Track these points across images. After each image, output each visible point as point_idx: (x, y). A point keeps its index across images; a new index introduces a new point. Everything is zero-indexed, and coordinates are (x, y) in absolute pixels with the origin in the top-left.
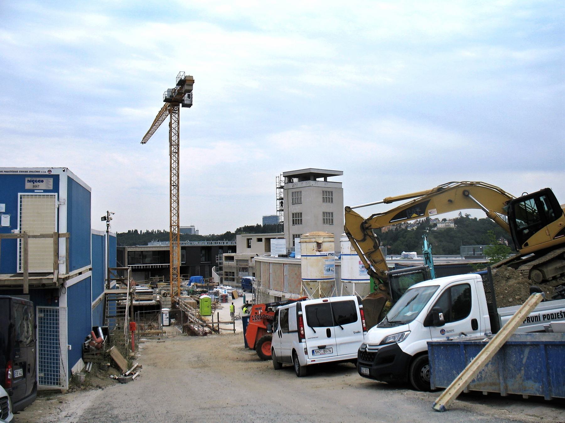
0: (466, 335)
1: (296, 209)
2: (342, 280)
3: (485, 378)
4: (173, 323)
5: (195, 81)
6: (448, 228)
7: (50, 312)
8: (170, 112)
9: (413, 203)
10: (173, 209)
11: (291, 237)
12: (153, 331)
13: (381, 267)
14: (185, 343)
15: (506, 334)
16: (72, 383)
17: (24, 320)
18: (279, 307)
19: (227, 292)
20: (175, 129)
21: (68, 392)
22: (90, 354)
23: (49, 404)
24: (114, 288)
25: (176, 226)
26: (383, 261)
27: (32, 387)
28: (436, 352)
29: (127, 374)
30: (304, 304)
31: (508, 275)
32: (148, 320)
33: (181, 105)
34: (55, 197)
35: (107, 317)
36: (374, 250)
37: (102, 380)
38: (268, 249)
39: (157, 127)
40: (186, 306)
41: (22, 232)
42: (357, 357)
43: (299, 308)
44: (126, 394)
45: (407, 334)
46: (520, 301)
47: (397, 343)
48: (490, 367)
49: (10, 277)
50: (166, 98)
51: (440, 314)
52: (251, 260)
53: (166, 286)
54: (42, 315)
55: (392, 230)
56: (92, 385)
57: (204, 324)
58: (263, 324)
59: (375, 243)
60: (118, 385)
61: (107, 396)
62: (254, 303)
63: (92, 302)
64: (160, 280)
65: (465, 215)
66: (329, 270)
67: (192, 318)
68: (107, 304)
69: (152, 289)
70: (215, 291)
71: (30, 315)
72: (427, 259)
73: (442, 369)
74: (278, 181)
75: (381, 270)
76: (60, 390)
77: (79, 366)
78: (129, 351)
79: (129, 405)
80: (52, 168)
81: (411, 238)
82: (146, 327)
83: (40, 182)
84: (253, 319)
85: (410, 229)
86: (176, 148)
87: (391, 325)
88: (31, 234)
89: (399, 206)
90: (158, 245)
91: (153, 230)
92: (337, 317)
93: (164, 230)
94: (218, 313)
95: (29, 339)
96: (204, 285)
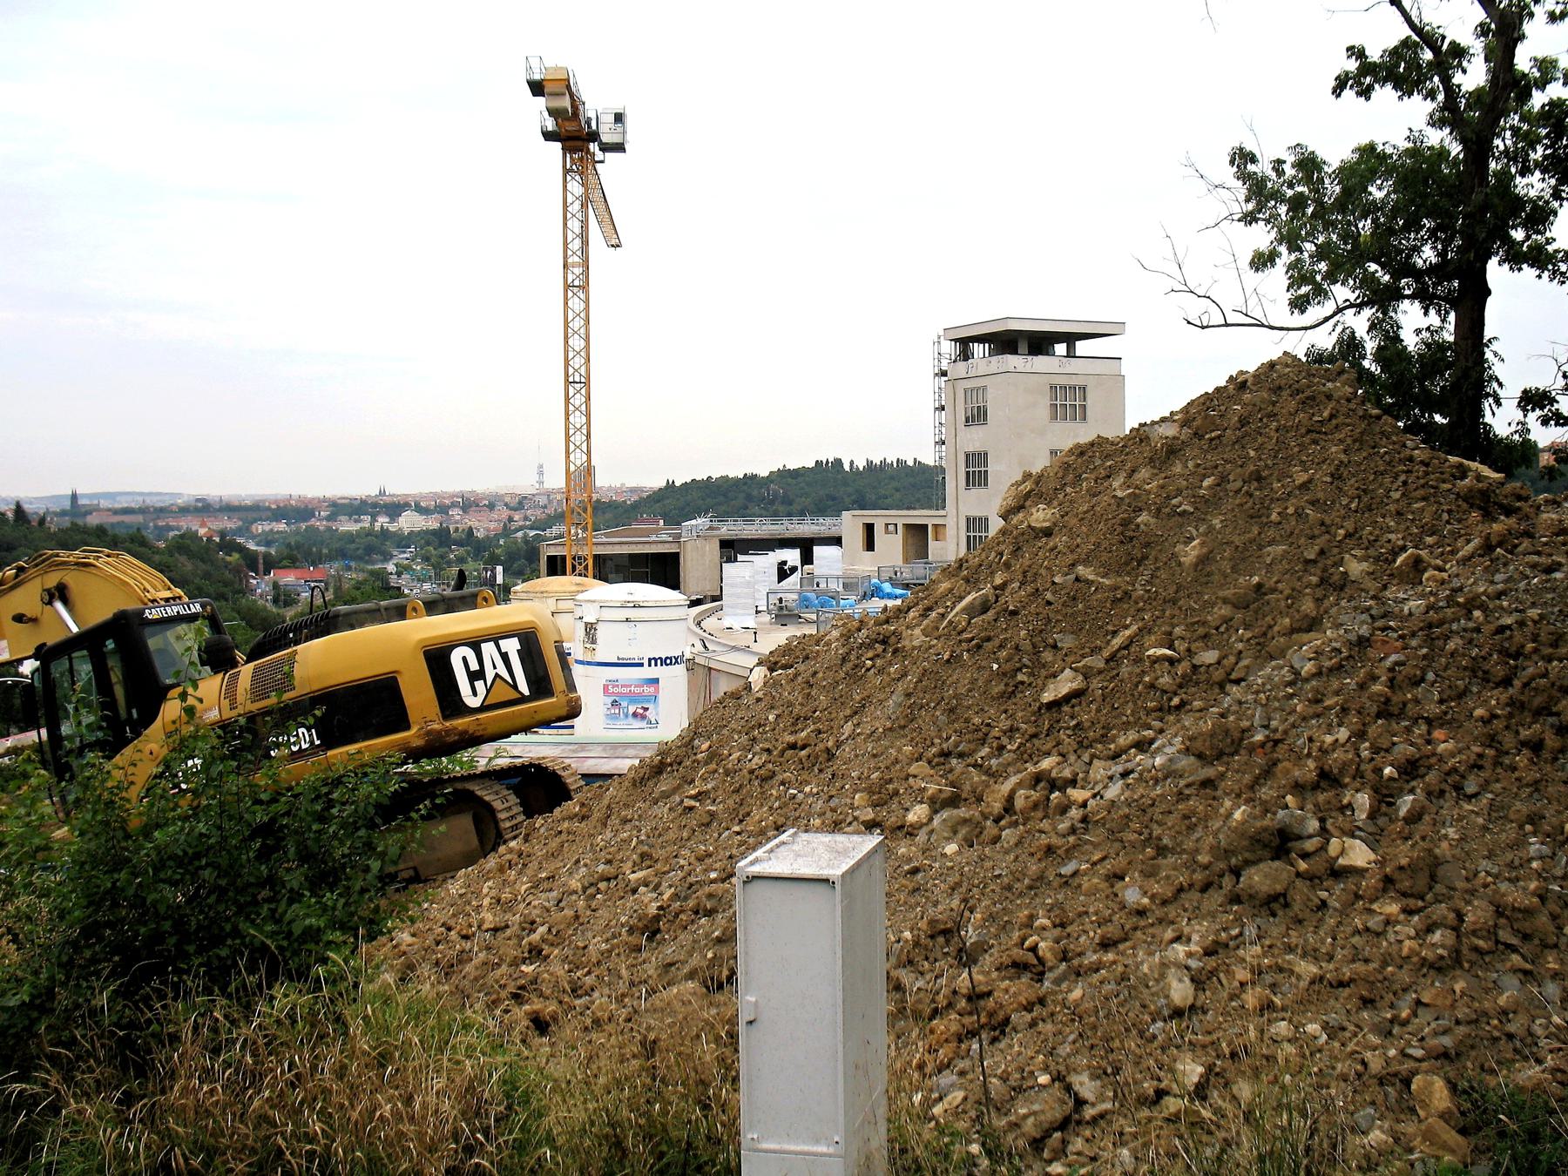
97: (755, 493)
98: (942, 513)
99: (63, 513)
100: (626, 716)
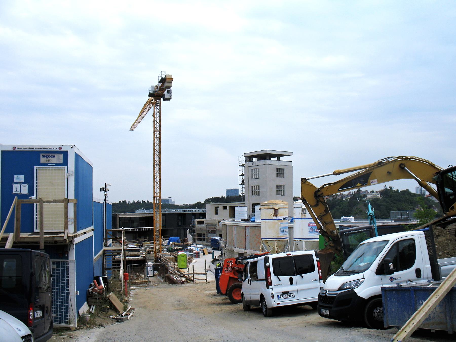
0: (412, 282)
1: (255, 183)
2: (294, 239)
3: (434, 318)
4: (156, 274)
5: (173, 79)
6: (375, 198)
7: (62, 264)
8: (154, 105)
9: (358, 174)
10: (156, 183)
11: (251, 205)
12: (140, 280)
13: (330, 227)
14: (167, 290)
15: (452, 281)
16: (80, 321)
17: (42, 270)
18: (248, 260)
19: (199, 250)
20: (157, 118)
21: (76, 329)
22: (94, 299)
23: (62, 339)
24: (110, 246)
25: (158, 196)
26: (332, 222)
27: (49, 325)
28: (388, 296)
29: (124, 314)
30: (271, 257)
31: (437, 233)
32: (136, 272)
33: (162, 99)
34: (64, 170)
35: (105, 269)
36: (325, 213)
37: (103, 320)
38: (232, 215)
39: (143, 117)
40: (166, 260)
41: (38, 198)
42: (318, 300)
43: (267, 260)
44: (124, 331)
45: (361, 281)
46: (448, 254)
47: (353, 289)
48: (438, 309)
49: (29, 235)
50: (150, 93)
51: (390, 264)
52: (218, 224)
53: (150, 245)
54: (55, 266)
55: (330, 200)
56: (95, 324)
57: (182, 275)
58: (234, 275)
59: (326, 208)
60: (117, 323)
61: (108, 333)
62: (221, 258)
63: (94, 256)
64: (145, 240)
65: (389, 188)
66: (284, 231)
67: (171, 270)
68: (105, 259)
69: (139, 247)
70: (189, 249)
71: (47, 266)
72: (372, 220)
73: (394, 311)
74: (240, 161)
75: (331, 230)
76: (70, 327)
77: (85, 308)
78: (123, 296)
79: (128, 340)
80: (62, 145)
81: (345, 206)
82: (136, 278)
83: (52, 157)
84: (225, 271)
85: (344, 199)
86: (158, 134)
87: (347, 274)
88: (45, 200)
89: (346, 177)
90: (144, 213)
91: (139, 201)
92: (298, 268)
93: (147, 201)
94: (193, 266)
95: (47, 286)
96: (180, 244)
98: (243, 202)
100: (314, 231)
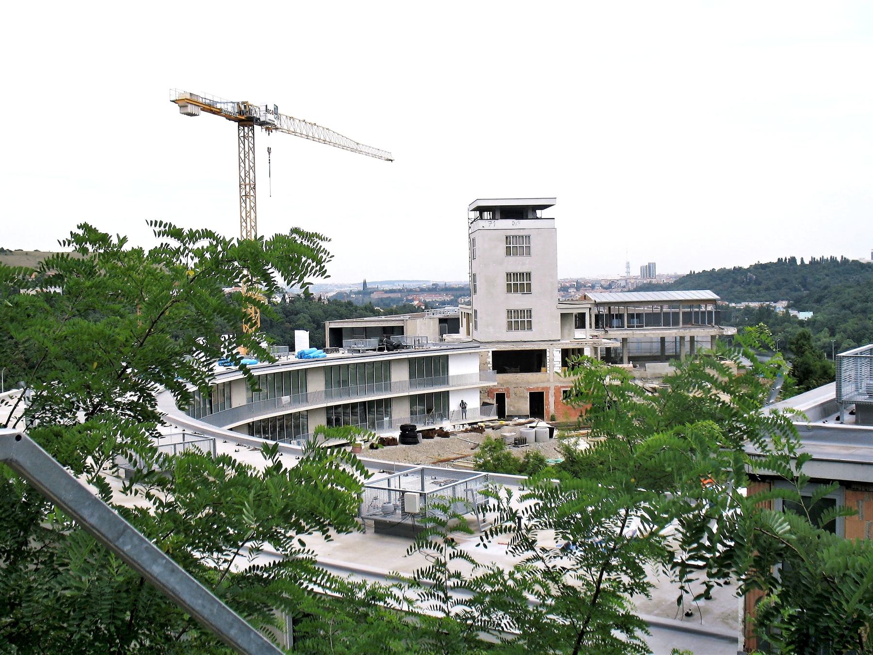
97: (739, 278)
99: (359, 293)
